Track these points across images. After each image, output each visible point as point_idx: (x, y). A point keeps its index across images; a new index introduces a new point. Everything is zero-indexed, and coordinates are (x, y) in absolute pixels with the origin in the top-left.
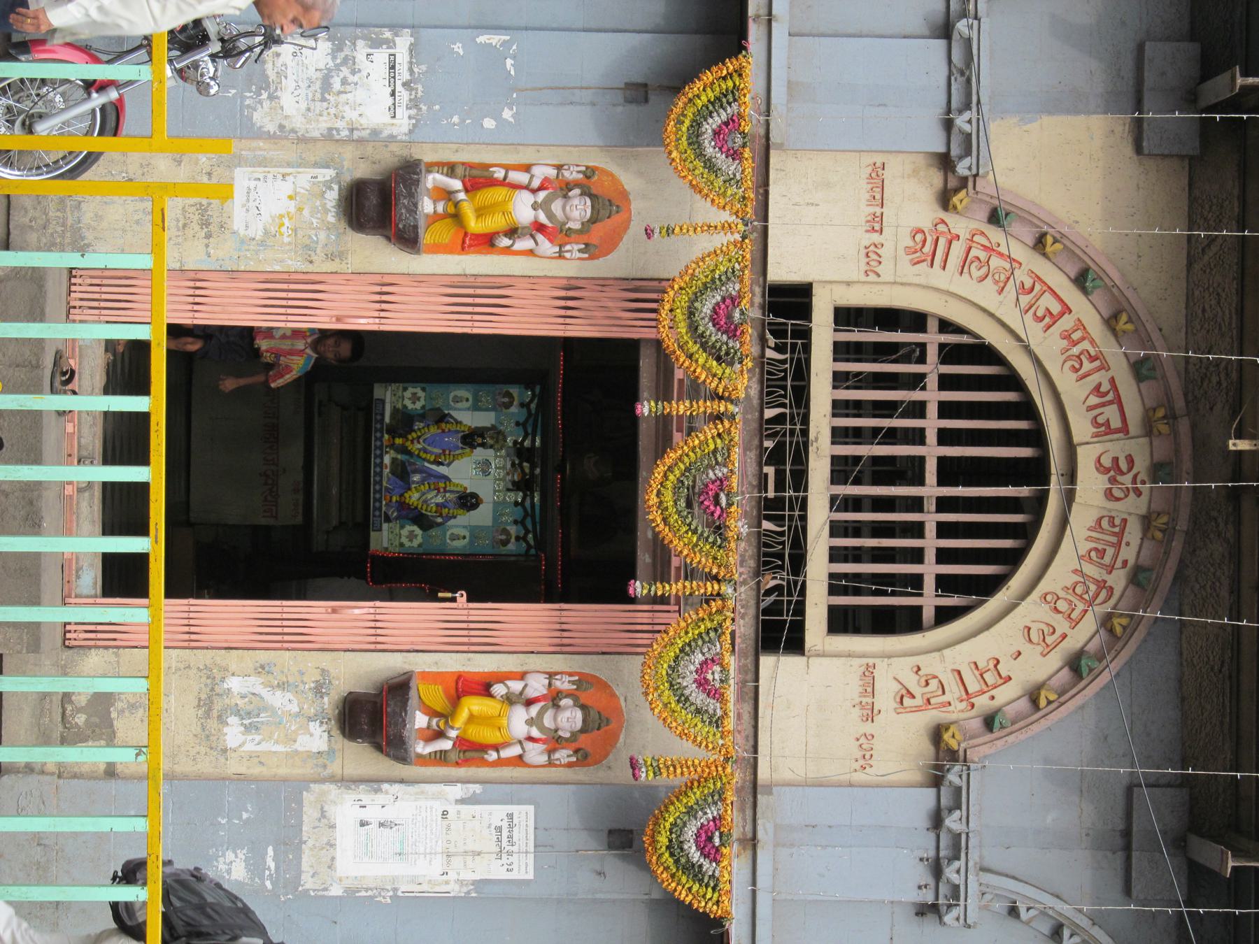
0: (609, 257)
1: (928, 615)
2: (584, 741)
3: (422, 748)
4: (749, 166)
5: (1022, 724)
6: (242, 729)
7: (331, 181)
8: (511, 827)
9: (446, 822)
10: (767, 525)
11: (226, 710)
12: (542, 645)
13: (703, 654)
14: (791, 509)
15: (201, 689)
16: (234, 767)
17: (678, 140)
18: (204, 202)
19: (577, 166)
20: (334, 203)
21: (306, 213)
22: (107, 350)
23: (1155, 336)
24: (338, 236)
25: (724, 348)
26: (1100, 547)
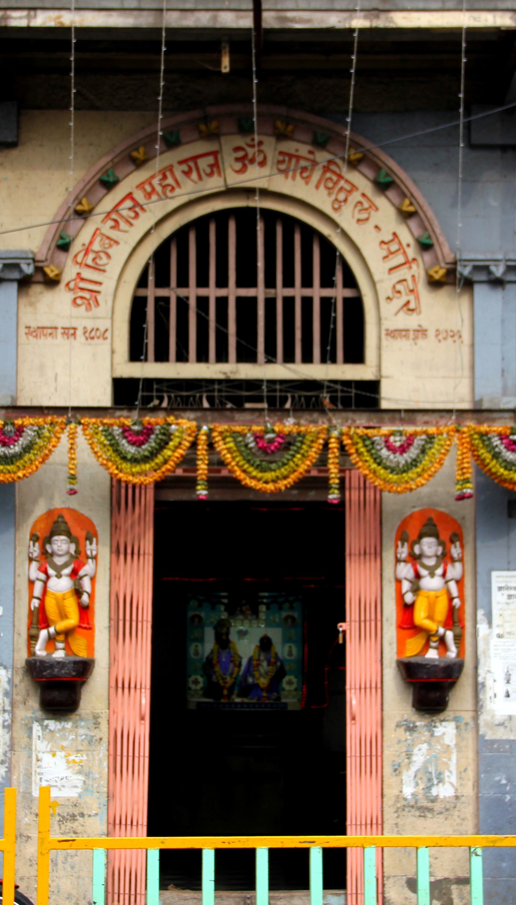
0: (95, 523)
1: (349, 293)
2: (445, 536)
3: (452, 653)
4: (28, 421)
5: (427, 224)
6: (440, 784)
7: (42, 725)
8: (508, 588)
9: (506, 636)
10: (288, 405)
11: (427, 796)
12: (376, 568)
13: (381, 449)
14: (275, 391)
15: (412, 815)
16: (469, 790)
17: (9, 472)
18: (58, 818)
19: (29, 546)
20: (58, 723)
21: (65, 743)
22: (167, 889)
23: (148, 132)
24: (82, 719)
25: (160, 437)
26: (299, 171)
